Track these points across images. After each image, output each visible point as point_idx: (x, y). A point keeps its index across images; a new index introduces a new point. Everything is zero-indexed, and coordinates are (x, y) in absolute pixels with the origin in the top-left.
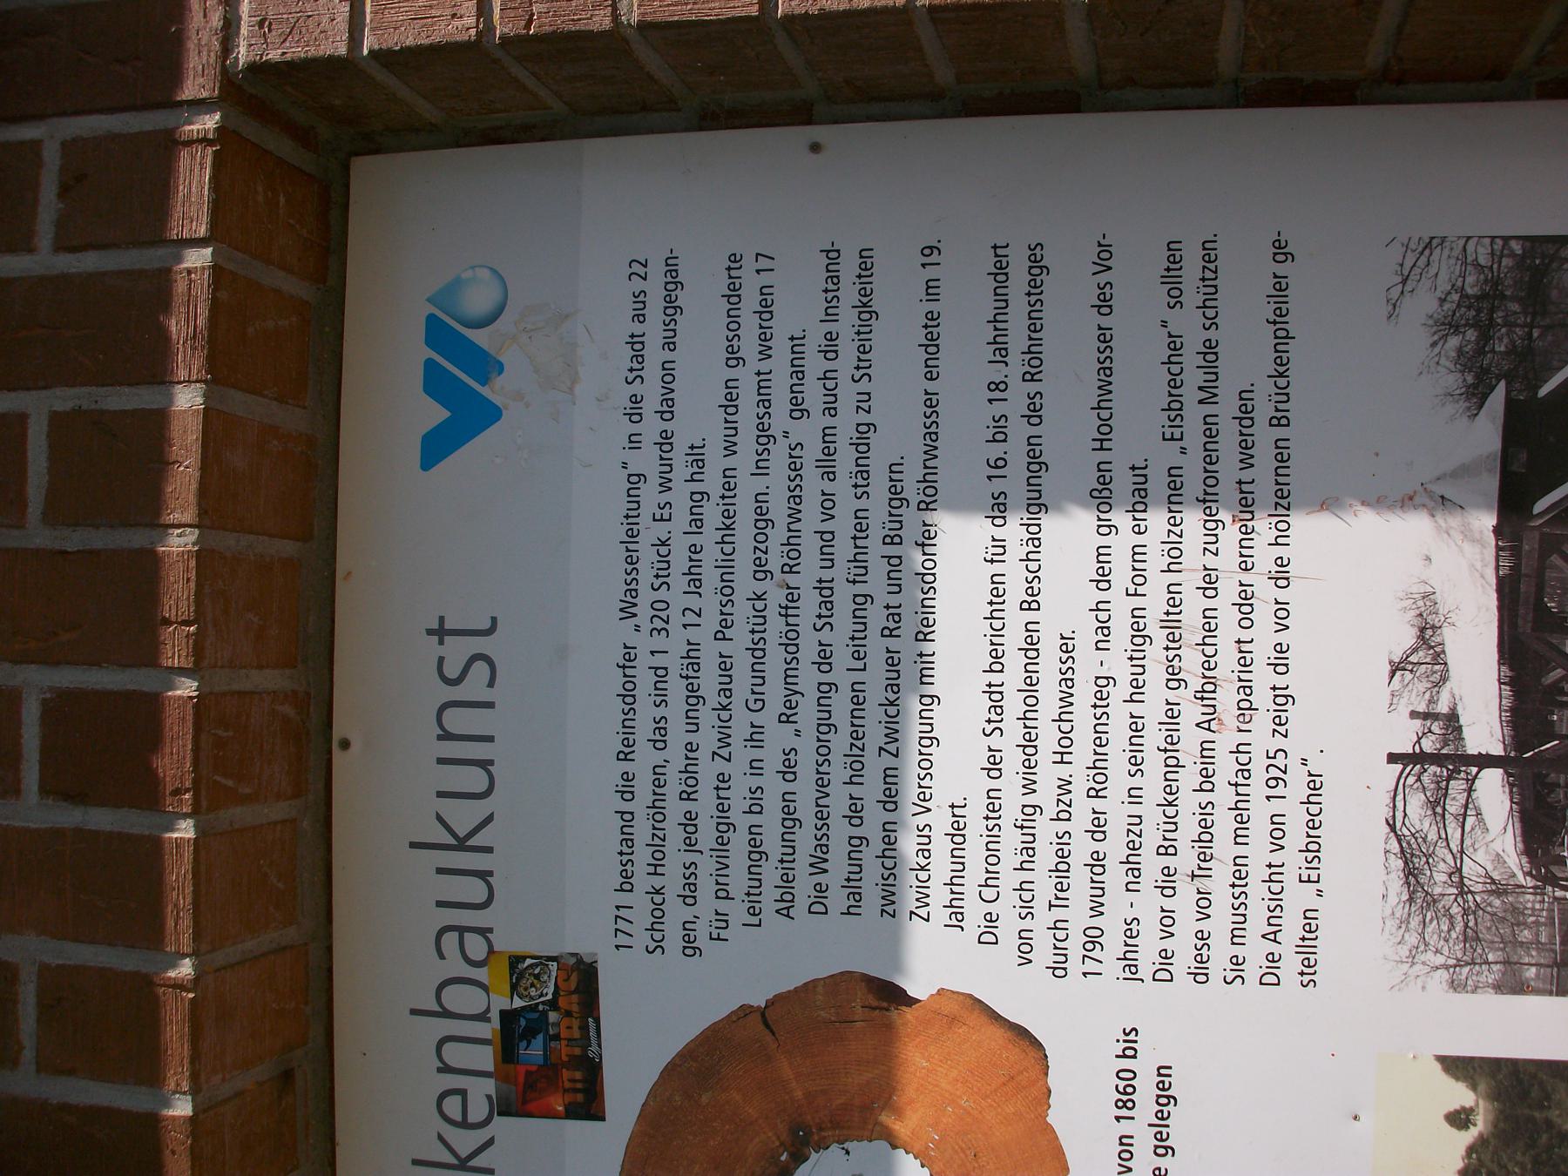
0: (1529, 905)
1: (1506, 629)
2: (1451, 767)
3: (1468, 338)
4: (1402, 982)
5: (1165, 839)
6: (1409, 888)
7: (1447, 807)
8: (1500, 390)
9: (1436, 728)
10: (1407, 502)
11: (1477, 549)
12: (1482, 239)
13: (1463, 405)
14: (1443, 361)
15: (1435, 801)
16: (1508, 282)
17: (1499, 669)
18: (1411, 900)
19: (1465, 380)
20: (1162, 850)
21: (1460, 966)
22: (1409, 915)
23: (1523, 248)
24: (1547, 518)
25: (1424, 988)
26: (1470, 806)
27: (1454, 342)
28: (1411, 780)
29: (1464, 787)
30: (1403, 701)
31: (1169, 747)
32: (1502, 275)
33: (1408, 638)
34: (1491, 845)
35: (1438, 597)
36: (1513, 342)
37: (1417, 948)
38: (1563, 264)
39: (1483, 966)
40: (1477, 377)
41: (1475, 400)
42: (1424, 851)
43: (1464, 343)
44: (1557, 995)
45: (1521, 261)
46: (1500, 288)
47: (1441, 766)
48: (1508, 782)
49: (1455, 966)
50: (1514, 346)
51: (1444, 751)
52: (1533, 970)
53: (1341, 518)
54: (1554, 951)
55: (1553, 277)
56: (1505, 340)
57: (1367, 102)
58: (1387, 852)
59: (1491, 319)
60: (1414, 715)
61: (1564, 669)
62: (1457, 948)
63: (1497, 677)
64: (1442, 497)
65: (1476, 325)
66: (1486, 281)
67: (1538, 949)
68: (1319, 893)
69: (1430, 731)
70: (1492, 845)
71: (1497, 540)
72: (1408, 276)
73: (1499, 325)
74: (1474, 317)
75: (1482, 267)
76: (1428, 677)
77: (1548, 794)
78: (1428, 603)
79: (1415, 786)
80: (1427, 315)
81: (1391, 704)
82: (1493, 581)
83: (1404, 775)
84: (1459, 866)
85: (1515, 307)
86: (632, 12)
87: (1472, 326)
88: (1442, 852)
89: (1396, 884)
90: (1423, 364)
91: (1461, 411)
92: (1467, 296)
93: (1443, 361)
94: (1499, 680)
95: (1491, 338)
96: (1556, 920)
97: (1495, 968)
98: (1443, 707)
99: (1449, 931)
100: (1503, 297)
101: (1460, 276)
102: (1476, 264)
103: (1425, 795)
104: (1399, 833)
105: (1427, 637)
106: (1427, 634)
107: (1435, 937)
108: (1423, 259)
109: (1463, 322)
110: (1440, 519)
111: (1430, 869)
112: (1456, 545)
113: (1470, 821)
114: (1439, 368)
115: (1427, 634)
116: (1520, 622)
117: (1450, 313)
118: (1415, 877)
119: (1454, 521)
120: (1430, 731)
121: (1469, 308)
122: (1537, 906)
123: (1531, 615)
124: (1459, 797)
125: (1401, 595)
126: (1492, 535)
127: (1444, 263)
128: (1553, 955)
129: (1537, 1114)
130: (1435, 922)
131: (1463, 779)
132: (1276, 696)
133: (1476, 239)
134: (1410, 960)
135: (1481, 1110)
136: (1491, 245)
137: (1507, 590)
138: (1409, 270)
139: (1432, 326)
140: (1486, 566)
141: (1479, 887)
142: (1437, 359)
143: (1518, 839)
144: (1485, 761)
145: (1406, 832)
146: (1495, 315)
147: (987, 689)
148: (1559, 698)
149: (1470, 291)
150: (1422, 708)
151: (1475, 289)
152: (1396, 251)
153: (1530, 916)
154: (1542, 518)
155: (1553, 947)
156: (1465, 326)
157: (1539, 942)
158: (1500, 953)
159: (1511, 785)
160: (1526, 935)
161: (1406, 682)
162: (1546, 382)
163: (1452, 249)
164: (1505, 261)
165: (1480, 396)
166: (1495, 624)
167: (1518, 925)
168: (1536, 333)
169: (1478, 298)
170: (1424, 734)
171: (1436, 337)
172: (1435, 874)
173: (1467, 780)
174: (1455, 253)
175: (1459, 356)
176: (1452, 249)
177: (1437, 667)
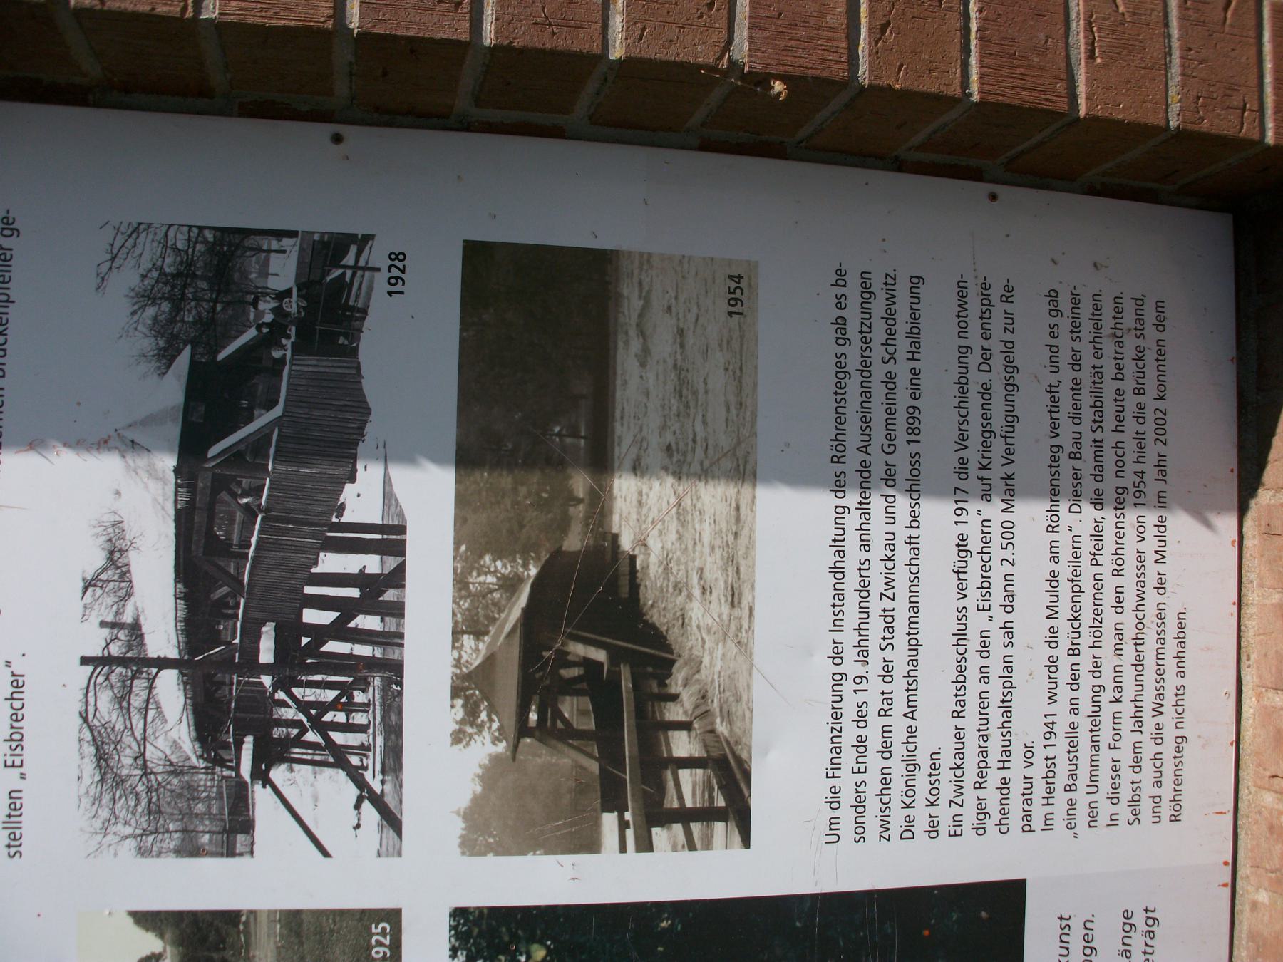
0: (202, 783)
1: (181, 552)
2: (135, 668)
3: (162, 309)
4: (97, 850)
5: (1073, 644)
6: (101, 770)
7: (132, 702)
8: (187, 352)
9: (122, 635)
10: (103, 444)
11: (160, 485)
12: (181, 228)
13: (154, 364)
14: (140, 327)
15: (122, 697)
16: (200, 264)
17: (176, 586)
18: (102, 780)
19: (157, 344)
20: (1071, 652)
21: (147, 835)
22: (101, 793)
23: (215, 237)
24: (219, 461)
25: (115, 854)
26: (151, 701)
27: (151, 311)
28: (101, 679)
29: (146, 684)
30: (94, 613)
31: (1075, 579)
32: (195, 258)
33: (99, 559)
34: (169, 733)
35: (125, 525)
36: (199, 314)
37: (109, 821)
38: (246, 252)
39: (166, 835)
40: (167, 342)
41: (165, 361)
42: (113, 739)
43: (160, 313)
44: (227, 856)
45: (212, 249)
46: (193, 268)
47: (126, 667)
48: (182, 681)
49: (142, 835)
50: (201, 318)
51: (129, 655)
52: (207, 836)
53: (48, 459)
54: (223, 820)
55: (237, 263)
56: (194, 312)
57: (98, 105)
58: (80, 740)
59: (183, 294)
60: (103, 624)
61: (229, 587)
62: (143, 820)
63: (173, 593)
64: (133, 441)
65: (170, 298)
66: (181, 262)
67: (209, 819)
68: (23, 776)
69: (117, 638)
70: (170, 734)
71: (177, 478)
72: (117, 254)
73: (189, 299)
74: (169, 291)
75: (179, 250)
76: (115, 592)
77: (216, 691)
78: (117, 530)
79: (105, 684)
80: (130, 288)
81: (84, 615)
82: (172, 512)
83: (95, 675)
84: (142, 750)
85: (204, 285)
86: (211, 11)
87: (166, 299)
88: (127, 739)
89: (89, 767)
90: (123, 329)
91: (152, 369)
92: (165, 274)
93: (140, 327)
94: (175, 596)
95: (181, 309)
96: (225, 796)
97: (176, 835)
98: (128, 618)
99: (136, 806)
100: (194, 276)
101: (161, 257)
102: (176, 249)
103: (113, 691)
104: (91, 724)
105: (116, 558)
106: (116, 557)
107: (124, 811)
108: (131, 242)
109: (160, 295)
110: (129, 459)
111: (118, 754)
112: (143, 482)
113: (151, 714)
114: (137, 333)
115: (116, 557)
116: (193, 547)
117: (149, 287)
118: (106, 761)
119: (141, 461)
120: (117, 638)
121: (165, 284)
122: (209, 784)
123: (203, 541)
124: (142, 693)
125: (95, 523)
126: (172, 474)
127: (148, 245)
128: (223, 824)
129: (215, 956)
130: (124, 799)
131: (144, 678)
132: (960, 551)
133: (176, 227)
134: (103, 831)
135: (168, 954)
136: (189, 232)
137: (184, 520)
138: (117, 249)
139: (133, 298)
140: (166, 500)
141: (160, 769)
142: (135, 325)
143: (192, 728)
144: (163, 663)
145: (96, 722)
146: (187, 291)
147: (882, 613)
148: (225, 611)
149: (167, 270)
150: (110, 618)
151: (172, 268)
152: (109, 233)
153: (203, 791)
154: (214, 460)
155: (223, 817)
156: (161, 298)
157: (210, 814)
158: (179, 823)
159: (185, 683)
160: (200, 808)
161: (97, 596)
162: (224, 348)
163: (155, 234)
164: (199, 247)
165: (169, 357)
166: (173, 548)
167: (193, 799)
168: (219, 307)
169: (174, 276)
170: (112, 640)
171: (136, 307)
172: (122, 758)
173: (149, 679)
174: (158, 238)
175: (154, 324)
176: (155, 234)
177: (123, 584)
